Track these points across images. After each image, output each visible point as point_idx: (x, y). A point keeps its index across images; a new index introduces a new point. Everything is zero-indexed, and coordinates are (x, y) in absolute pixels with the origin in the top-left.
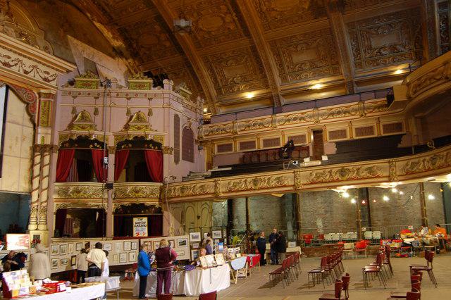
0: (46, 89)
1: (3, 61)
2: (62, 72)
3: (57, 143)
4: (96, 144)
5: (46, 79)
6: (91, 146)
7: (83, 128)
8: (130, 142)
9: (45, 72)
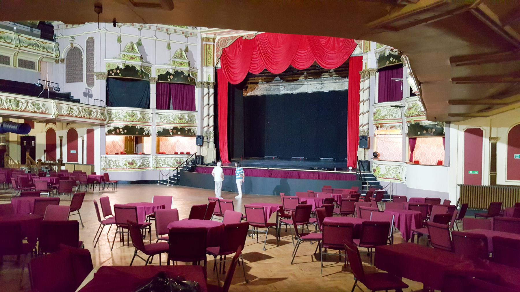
6: (388, 62)
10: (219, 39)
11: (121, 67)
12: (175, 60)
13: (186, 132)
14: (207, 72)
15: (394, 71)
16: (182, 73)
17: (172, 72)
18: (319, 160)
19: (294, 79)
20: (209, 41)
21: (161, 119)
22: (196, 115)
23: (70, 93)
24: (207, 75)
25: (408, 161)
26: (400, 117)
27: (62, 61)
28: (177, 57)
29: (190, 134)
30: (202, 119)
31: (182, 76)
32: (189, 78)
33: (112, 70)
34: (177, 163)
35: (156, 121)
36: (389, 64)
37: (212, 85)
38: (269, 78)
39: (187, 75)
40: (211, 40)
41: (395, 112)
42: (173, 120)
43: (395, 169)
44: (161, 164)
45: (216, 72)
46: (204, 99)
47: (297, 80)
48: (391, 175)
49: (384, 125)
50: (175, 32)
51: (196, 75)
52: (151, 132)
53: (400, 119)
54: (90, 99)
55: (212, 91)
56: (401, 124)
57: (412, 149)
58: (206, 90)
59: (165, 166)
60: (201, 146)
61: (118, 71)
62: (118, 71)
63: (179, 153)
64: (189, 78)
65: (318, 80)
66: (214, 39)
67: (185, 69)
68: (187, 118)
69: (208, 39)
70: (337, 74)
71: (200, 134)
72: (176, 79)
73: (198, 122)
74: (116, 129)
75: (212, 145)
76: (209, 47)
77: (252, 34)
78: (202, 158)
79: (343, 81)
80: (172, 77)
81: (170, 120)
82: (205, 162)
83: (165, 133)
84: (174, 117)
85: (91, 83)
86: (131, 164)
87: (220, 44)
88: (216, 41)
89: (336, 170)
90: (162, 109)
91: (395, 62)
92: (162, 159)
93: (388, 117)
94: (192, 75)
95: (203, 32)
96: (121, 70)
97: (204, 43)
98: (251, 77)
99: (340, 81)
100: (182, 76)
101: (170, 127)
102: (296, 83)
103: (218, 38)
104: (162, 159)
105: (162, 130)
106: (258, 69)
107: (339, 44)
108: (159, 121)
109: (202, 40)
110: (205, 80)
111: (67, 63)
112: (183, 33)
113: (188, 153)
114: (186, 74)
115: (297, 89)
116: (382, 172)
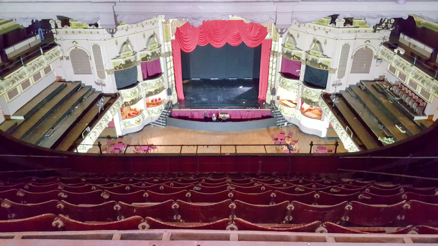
11: (123, 63)
16: (155, 52)
17: (150, 54)
23: (91, 86)
24: (167, 47)
27: (67, 58)
33: (117, 67)
52: (142, 96)
54: (103, 87)
59: (153, 114)
61: (121, 66)
62: (121, 66)
72: (152, 58)
74: (125, 103)
85: (101, 75)
86: (139, 121)
96: (123, 65)
101: (152, 90)
105: (148, 93)
110: (167, 51)
111: (71, 60)
116: (285, 112)
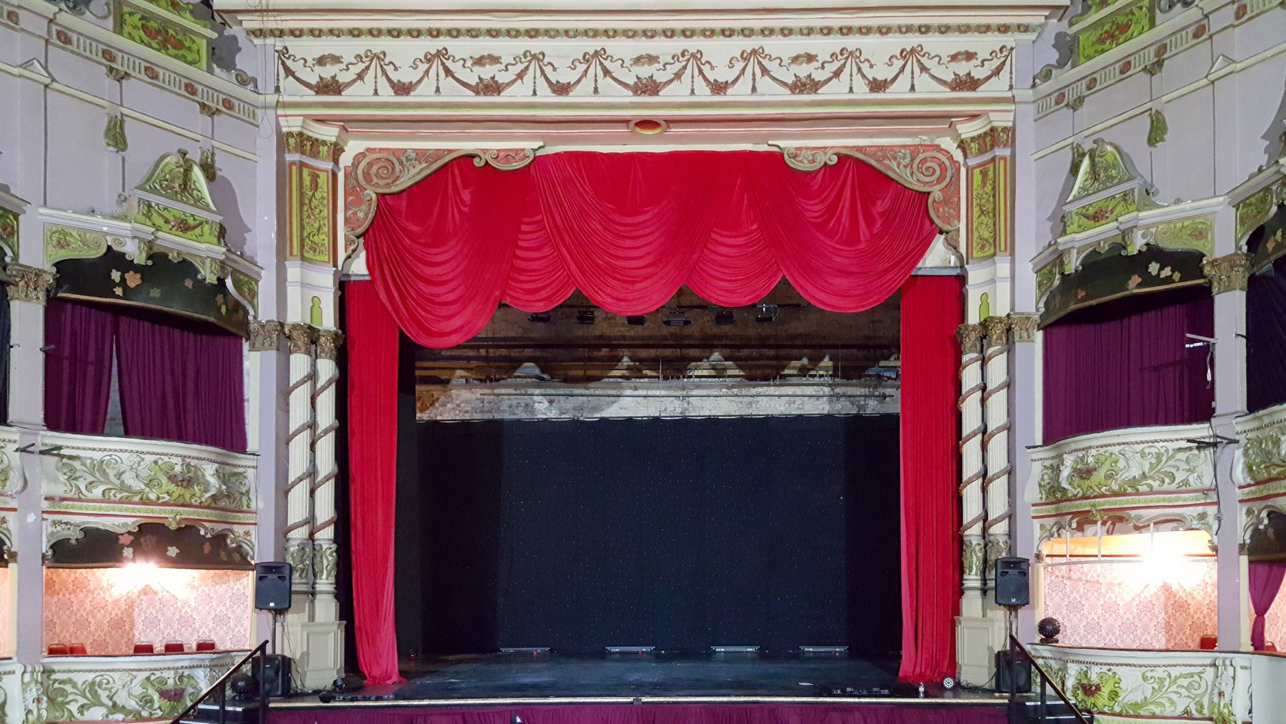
0: (974, 117)
1: (473, 81)
2: (1025, 29)
3: (1030, 302)
4: (1154, 268)
5: (801, 86)
6: (1136, 279)
7: (1097, 217)
8: (131, 629)
9: (321, 61)
10: (363, 155)
12: (154, 199)
13: (207, 548)
14: (304, 285)
15: (1165, 311)
16: (186, 268)
17: (134, 251)
18: (709, 656)
19: (589, 373)
20: (315, 154)
21: (73, 478)
22: (250, 473)
25: (1251, 649)
26: (1208, 481)
28: (166, 189)
29: (223, 555)
30: (283, 490)
31: (189, 283)
32: (220, 298)
34: (163, 694)
35: (46, 488)
36: (1139, 286)
37: (327, 344)
38: (495, 364)
39: (211, 279)
40: (324, 149)
41: (1183, 466)
42: (138, 485)
43: (1185, 682)
44: (74, 708)
45: (344, 287)
46: (290, 407)
47: (599, 379)
48: (1172, 702)
49: (1133, 513)
50: (151, 72)
51: (253, 294)
53: (1205, 492)
55: (327, 368)
56: (1212, 511)
57: (1261, 607)
58: (299, 364)
60: (279, 612)
63: (158, 647)
64: (220, 298)
65: (675, 382)
66: (337, 150)
67: (204, 251)
68: (213, 481)
69: (308, 144)
70: (740, 367)
71: (270, 558)
72: (156, 293)
73: (261, 502)
75: (327, 608)
76: (315, 178)
77: (517, 151)
78: (286, 664)
79: (753, 391)
80: (133, 280)
81: (123, 487)
82: (297, 684)
83: (96, 548)
84: (145, 473)
87: (367, 175)
88: (346, 160)
89: (926, 695)
90: (73, 426)
91: (1169, 280)
92: (80, 679)
93: (1155, 485)
94: (236, 284)
95: (286, 105)
97: (289, 157)
98: (421, 360)
99: (744, 392)
100: (189, 283)
101: (120, 520)
102: (595, 388)
103: (353, 147)
104: (80, 679)
106: (544, 294)
107: (870, 222)
108: (59, 490)
109: (283, 141)
110: (295, 315)
112: (191, 89)
113: (204, 647)
114: (209, 275)
115: (594, 409)
